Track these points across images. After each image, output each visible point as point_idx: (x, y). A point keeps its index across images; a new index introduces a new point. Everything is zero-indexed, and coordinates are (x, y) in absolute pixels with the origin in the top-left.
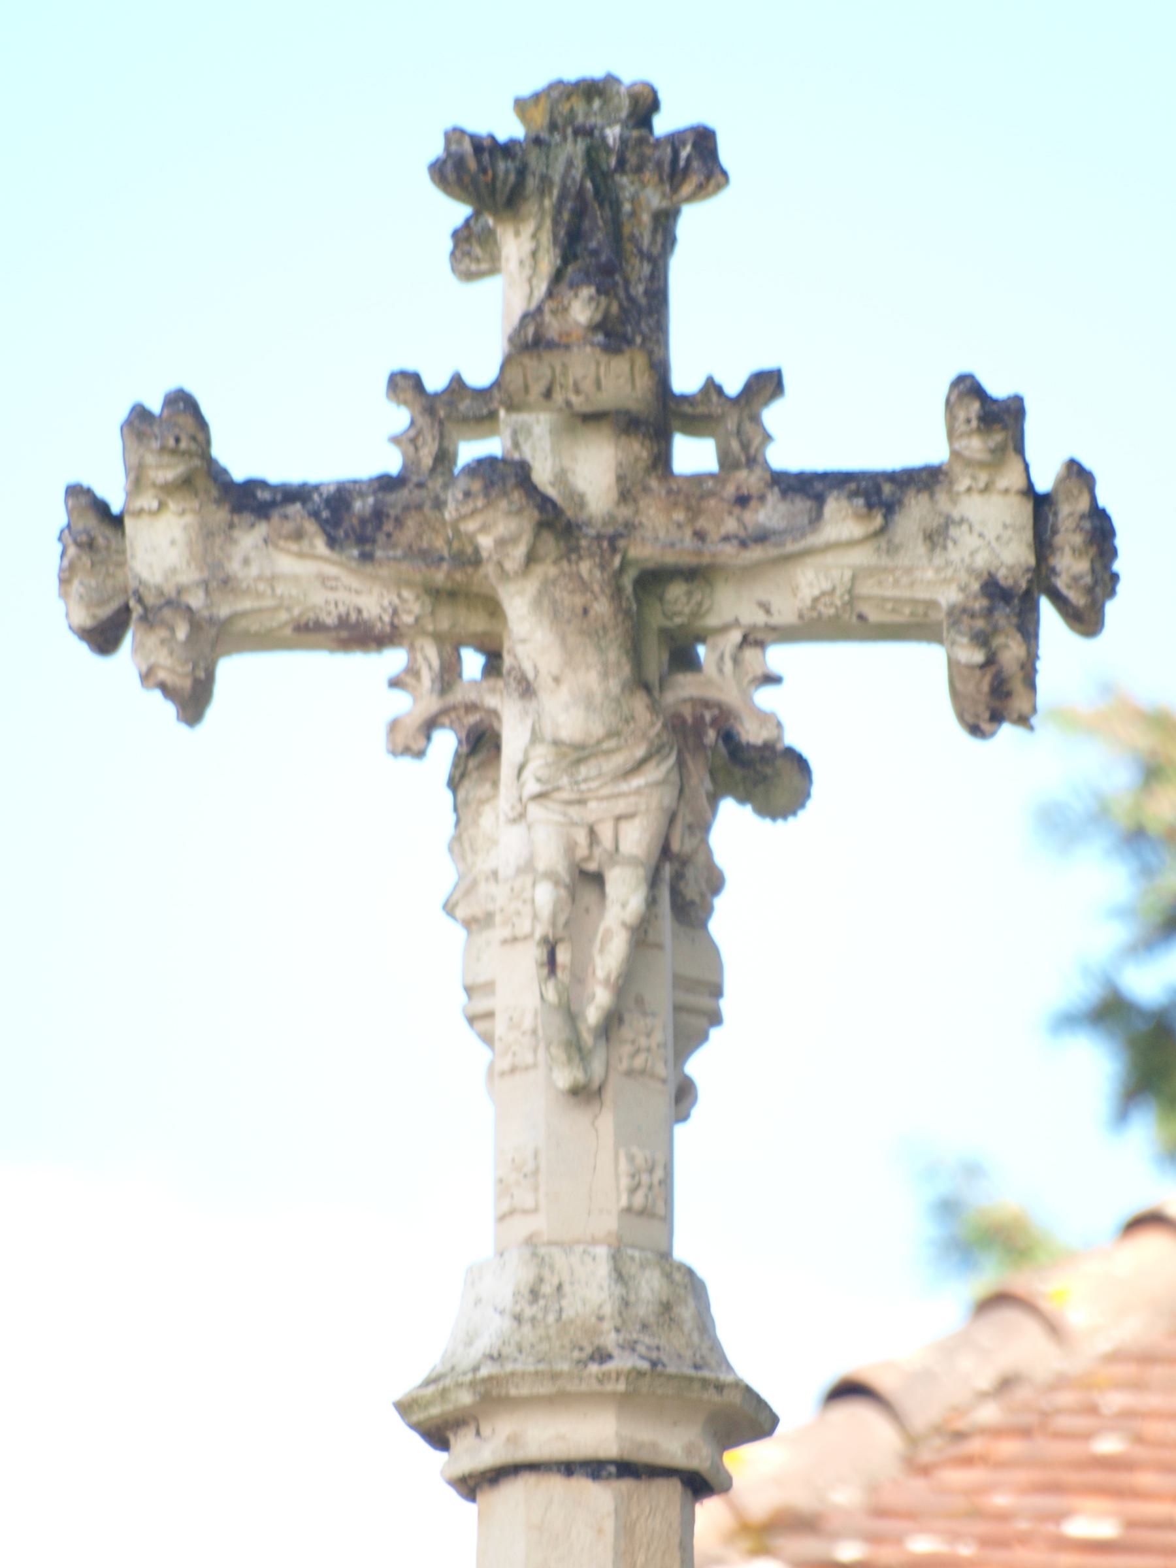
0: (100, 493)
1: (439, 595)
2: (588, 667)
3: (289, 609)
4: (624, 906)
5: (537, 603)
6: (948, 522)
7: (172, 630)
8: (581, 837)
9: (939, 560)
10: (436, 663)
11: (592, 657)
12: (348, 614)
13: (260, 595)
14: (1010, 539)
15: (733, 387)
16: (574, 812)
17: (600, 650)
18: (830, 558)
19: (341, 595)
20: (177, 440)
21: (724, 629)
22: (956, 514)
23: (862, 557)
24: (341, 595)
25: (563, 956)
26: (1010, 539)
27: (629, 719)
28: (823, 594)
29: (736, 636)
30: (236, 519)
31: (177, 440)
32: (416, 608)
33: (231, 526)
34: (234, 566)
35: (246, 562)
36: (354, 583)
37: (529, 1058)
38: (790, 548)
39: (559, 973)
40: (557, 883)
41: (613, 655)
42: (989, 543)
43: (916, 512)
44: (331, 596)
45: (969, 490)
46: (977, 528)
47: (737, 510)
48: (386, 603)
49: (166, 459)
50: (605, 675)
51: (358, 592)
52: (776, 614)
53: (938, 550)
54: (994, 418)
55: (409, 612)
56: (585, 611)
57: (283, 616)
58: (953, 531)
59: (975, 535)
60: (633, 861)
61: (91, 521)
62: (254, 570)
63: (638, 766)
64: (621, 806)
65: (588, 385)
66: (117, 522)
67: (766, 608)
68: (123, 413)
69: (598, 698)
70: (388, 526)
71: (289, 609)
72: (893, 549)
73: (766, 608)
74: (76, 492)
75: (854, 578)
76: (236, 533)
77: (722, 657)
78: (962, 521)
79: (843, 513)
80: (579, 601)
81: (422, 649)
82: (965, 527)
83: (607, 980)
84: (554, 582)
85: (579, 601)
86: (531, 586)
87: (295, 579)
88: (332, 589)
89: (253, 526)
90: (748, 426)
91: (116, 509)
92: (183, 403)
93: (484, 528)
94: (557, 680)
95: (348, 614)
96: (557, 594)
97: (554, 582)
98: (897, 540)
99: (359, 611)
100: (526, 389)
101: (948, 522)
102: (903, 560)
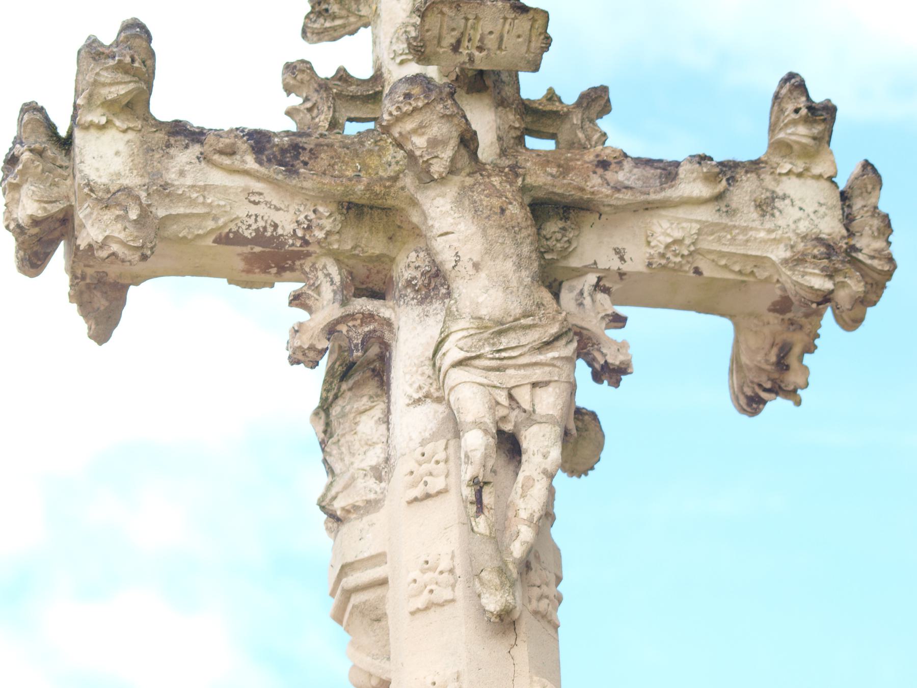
0: (53, 118)
1: (353, 210)
2: (506, 257)
3: (215, 218)
4: (545, 457)
5: (458, 202)
6: (774, 197)
7: (126, 210)
8: (503, 398)
9: (769, 225)
10: (337, 279)
11: (510, 250)
12: (265, 228)
13: (193, 202)
14: (825, 215)
15: (569, 97)
16: (494, 378)
17: (518, 244)
18: (681, 213)
19: (261, 210)
20: (133, 61)
21: (580, 273)
22: (780, 191)
23: (706, 214)
24: (261, 210)
25: (487, 499)
26: (825, 215)
27: (540, 305)
28: (675, 242)
29: (592, 279)
30: (172, 140)
31: (133, 61)
32: (328, 224)
33: (168, 146)
34: (171, 176)
35: (182, 173)
36: (271, 195)
37: (447, 594)
38: (571, 249)
39: (486, 511)
40: (486, 431)
41: (526, 249)
42: (809, 215)
43: (745, 191)
44: (254, 210)
45: (789, 173)
46: (798, 203)
47: (600, 171)
48: (301, 218)
49: (120, 76)
50: (519, 266)
51: (277, 209)
52: (629, 261)
53: (767, 217)
54: (806, 114)
55: (321, 228)
56: (503, 211)
57: (210, 224)
58: (778, 203)
59: (797, 209)
60: (549, 420)
61: (40, 140)
62: (189, 181)
63: (548, 344)
64: (538, 374)
65: (491, 42)
66: (66, 144)
67: (620, 254)
68: (81, 42)
69: (514, 283)
70: (304, 157)
71: (215, 218)
72: (731, 212)
73: (620, 254)
74: (32, 108)
75: (699, 233)
76: (172, 151)
77: (581, 293)
78: (784, 197)
79: (695, 175)
80: (496, 202)
81: (325, 267)
82: (787, 201)
83: (530, 520)
84: (471, 188)
85: (496, 202)
86: (451, 190)
87: (225, 189)
88: (255, 203)
89: (187, 147)
90: (587, 124)
91: (63, 132)
92: (136, 33)
93: (420, 129)
94: (476, 266)
95: (265, 228)
96: (476, 197)
97: (471, 188)
98: (734, 206)
99: (275, 226)
100: (440, 39)
101: (774, 197)
102: (740, 221)
